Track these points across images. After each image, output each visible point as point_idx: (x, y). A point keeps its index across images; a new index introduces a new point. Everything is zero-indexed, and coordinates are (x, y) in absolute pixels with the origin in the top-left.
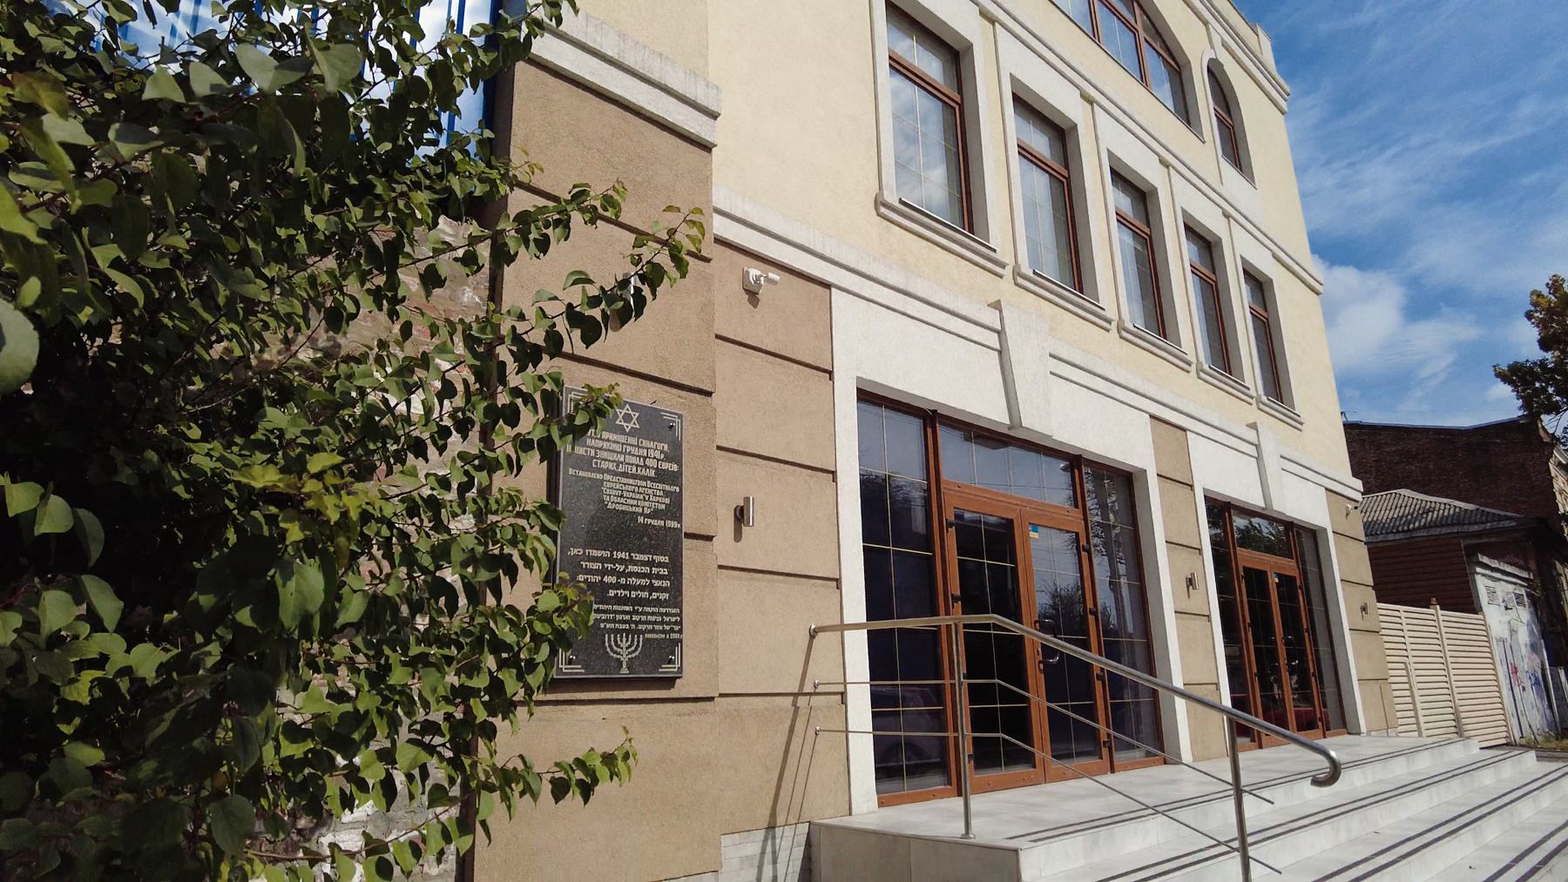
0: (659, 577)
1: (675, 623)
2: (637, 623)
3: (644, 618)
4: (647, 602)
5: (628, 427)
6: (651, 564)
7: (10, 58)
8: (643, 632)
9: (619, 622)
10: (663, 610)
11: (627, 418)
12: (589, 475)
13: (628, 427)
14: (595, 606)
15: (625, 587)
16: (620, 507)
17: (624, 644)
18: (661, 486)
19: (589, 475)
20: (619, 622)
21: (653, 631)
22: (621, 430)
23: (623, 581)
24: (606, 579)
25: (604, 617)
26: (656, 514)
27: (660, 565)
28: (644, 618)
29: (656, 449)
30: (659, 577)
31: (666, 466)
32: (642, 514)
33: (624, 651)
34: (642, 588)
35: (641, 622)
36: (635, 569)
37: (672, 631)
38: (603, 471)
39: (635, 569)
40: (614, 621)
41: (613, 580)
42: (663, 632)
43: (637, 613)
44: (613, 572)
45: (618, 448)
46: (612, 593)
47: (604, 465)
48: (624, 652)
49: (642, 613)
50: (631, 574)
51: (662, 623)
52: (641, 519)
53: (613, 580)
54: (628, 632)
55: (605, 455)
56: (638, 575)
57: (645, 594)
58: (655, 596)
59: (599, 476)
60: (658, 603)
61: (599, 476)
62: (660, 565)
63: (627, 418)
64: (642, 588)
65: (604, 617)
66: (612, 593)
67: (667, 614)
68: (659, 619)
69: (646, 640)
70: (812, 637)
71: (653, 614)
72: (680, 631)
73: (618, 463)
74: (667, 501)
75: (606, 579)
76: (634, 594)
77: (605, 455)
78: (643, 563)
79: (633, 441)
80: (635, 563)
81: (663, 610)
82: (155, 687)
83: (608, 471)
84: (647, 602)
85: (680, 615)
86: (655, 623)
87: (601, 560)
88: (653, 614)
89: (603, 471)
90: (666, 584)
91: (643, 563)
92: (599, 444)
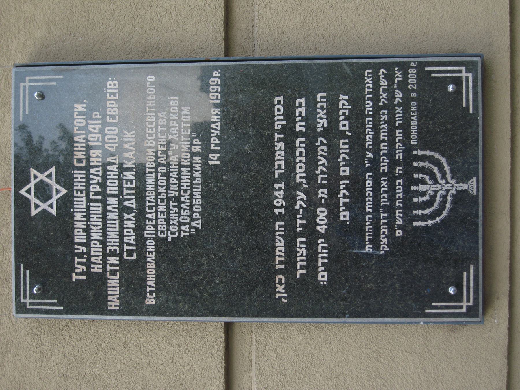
0: (310, 118)
1: (390, 78)
2: (393, 163)
3: (384, 148)
4: (357, 140)
5: (58, 191)
7: (396, 108)
8: (408, 151)
9: (392, 199)
10: (369, 105)
11: (43, 191)
12: (151, 266)
13: (58, 191)
14: (368, 249)
15: (334, 191)
16: (198, 202)
17: (429, 188)
18: (150, 118)
19: (151, 266)
20: (392, 199)
21: (406, 128)
23: (322, 193)
24: (322, 228)
25: (384, 230)
27: (289, 114)
28: (384, 148)
30: (310, 118)
32: (205, 158)
33: (440, 187)
34: (333, 154)
35: (391, 155)
36: (301, 169)
37: (403, 85)
38: (141, 241)
39: (301, 169)
40: (391, 209)
41: (322, 213)
42: (405, 105)
43: (375, 162)
45: (97, 211)
46: (345, 216)
47: (130, 237)
48: (442, 186)
49: (376, 151)
50: (311, 177)
51: (390, 107)
52: (214, 159)
53: (322, 213)
54: (410, 181)
55: (113, 235)
56: (312, 162)
57: (343, 145)
58: (344, 125)
59: (151, 245)
60: (357, 116)
61: (151, 245)
62: (289, 114)
64: (333, 154)
65: (384, 230)
66: (345, 216)
67: (376, 99)
68: (384, 115)
69: (423, 144)
70: (480, 56)
71: (376, 128)
72: (404, 67)
73: (123, 210)
74: (174, 101)
75: (322, 228)
76: (345, 171)
77: (113, 235)
78: (290, 149)
79: (79, 177)
80: (291, 167)
81: (369, 105)
82: (471, 114)
83: (139, 229)
84: (357, 140)
85: (376, 68)
86: (391, 122)
87: (290, 237)
88: (376, 128)
89: (141, 241)
91: (290, 149)
92: (96, 248)
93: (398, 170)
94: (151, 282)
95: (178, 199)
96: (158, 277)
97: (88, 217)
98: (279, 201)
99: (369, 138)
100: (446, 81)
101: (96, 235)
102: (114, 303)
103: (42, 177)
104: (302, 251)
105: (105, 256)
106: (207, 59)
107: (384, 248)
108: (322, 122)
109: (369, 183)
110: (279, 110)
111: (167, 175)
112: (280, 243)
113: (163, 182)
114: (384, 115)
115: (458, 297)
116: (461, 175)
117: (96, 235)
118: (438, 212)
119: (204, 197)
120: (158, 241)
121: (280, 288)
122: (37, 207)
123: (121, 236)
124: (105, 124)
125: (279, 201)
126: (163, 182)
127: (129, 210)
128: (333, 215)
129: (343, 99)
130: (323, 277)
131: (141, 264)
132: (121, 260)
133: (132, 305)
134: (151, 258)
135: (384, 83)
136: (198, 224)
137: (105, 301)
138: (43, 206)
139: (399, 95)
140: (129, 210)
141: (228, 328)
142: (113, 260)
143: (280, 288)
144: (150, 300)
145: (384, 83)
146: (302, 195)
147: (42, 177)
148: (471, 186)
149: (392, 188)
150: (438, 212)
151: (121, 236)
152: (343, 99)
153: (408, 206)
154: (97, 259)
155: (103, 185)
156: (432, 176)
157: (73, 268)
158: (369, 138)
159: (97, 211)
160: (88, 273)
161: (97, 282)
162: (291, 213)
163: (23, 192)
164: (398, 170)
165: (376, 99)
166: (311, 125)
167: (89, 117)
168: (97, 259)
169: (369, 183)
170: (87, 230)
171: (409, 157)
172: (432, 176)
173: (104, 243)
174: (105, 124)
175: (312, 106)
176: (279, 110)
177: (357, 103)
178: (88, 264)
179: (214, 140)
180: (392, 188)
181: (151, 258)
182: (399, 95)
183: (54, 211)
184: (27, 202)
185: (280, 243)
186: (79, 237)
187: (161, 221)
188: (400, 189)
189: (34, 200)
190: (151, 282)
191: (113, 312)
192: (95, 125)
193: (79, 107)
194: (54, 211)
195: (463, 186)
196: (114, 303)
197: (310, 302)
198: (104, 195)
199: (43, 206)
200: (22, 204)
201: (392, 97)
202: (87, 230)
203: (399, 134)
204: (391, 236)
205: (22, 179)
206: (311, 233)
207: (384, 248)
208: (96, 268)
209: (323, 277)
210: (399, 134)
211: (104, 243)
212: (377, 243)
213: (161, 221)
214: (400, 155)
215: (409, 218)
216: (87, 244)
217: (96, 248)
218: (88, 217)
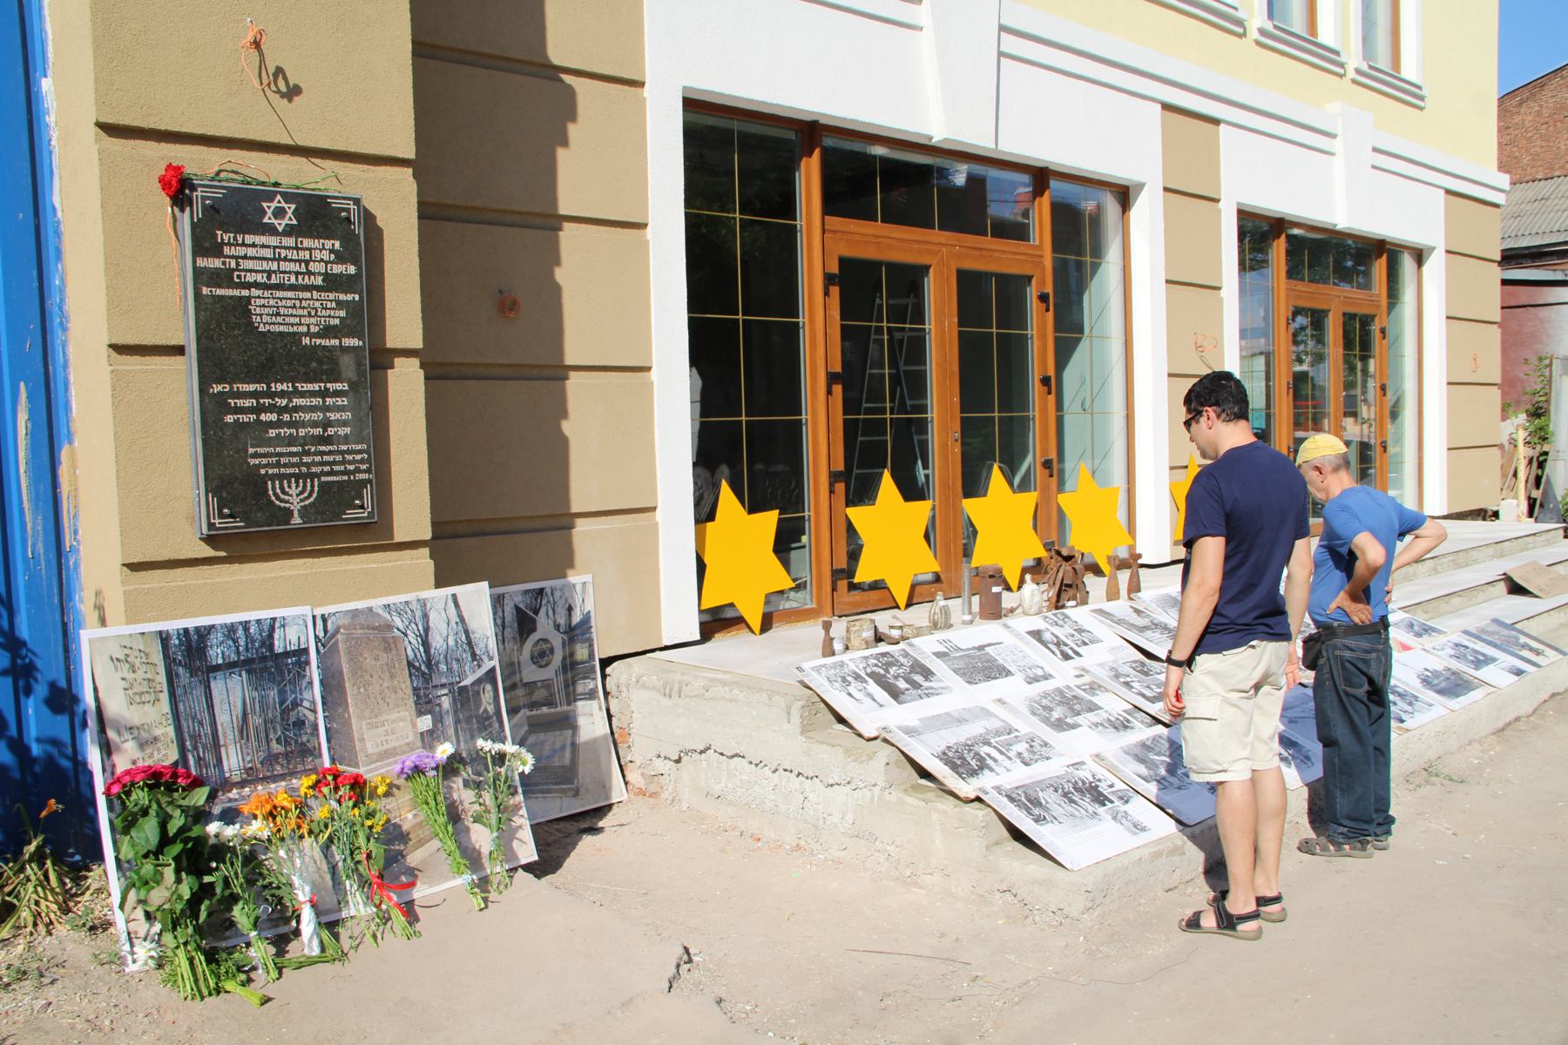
1: (362, 461)
2: (308, 465)
3: (318, 459)
6: (324, 394)
8: (318, 475)
9: (285, 466)
11: (280, 213)
14: (251, 450)
16: (277, 329)
17: (294, 491)
18: (332, 296)
20: (285, 466)
22: (271, 230)
23: (286, 417)
24: (263, 417)
25: (265, 461)
26: (328, 331)
27: (337, 394)
29: (321, 251)
31: (338, 269)
32: (308, 334)
33: (295, 499)
35: (314, 464)
38: (248, 286)
40: (278, 465)
41: (273, 417)
43: (308, 453)
44: (272, 408)
45: (268, 253)
46: (272, 433)
47: (250, 278)
49: (315, 454)
50: (296, 409)
51: (343, 462)
52: (306, 341)
53: (273, 417)
54: (297, 477)
55: (250, 264)
59: (245, 293)
61: (245, 293)
62: (337, 394)
63: (280, 213)
65: (265, 461)
67: (349, 452)
68: (339, 458)
69: (321, 485)
71: (330, 453)
73: (269, 273)
74: (342, 313)
75: (263, 417)
76: (302, 432)
77: (250, 264)
78: (313, 394)
80: (302, 395)
81: (344, 448)
83: (256, 285)
86: (335, 463)
88: (330, 453)
89: (248, 286)
90: (347, 415)
91: (313, 394)
92: (241, 251)
93: (304, 469)
94: (220, 292)
95: (278, 314)
96: (222, 297)
97: (263, 246)
98: (280, 387)
99: (323, 448)
100: (361, 499)
101: (251, 252)
102: (201, 262)
103: (290, 212)
104: (248, 403)
105: (236, 258)
106: (485, 383)
107: (252, 461)
108: (333, 416)
109: (294, 449)
110: (339, 386)
111: (294, 307)
112: (252, 387)
113: (289, 303)
114: (339, 458)
115: (221, 516)
116: (304, 511)
117: (251, 252)
118: (278, 498)
119: (280, 333)
120: (249, 298)
121: (220, 388)
122: (290, 219)
123: (250, 271)
124: (327, 263)
125: (280, 387)
126: (289, 303)
127: (269, 278)
128: (271, 425)
129: (348, 430)
130: (230, 419)
131: (231, 284)
132: (233, 270)
133: (200, 275)
134: (236, 293)
135: (359, 457)
136: (262, 329)
137: (203, 255)
138: (269, 212)
139: (352, 467)
140: (269, 278)
141: (179, 350)
142: (233, 265)
143: (220, 388)
144: (205, 291)
145: (359, 457)
146: (284, 402)
147: (290, 212)
148: (297, 520)
149: (293, 465)
150: (278, 498)
151: (250, 271)
152: (348, 430)
153: (281, 477)
154: (233, 251)
155: (285, 259)
156: (302, 492)
157: (226, 231)
158: (323, 448)
159: (268, 253)
160: (223, 244)
161: (216, 250)
162: (272, 395)
163: (279, 197)
164: (304, 469)
165: (349, 452)
166: (328, 409)
167: (332, 251)
168: (233, 251)
169: (294, 449)
170: (254, 245)
171: (312, 476)
172: (302, 492)
173: (245, 257)
174: (327, 263)
175: (342, 409)
176: (339, 386)
177: (346, 439)
178: (229, 244)
179: (318, 341)
180: (293, 465)
181: (236, 293)
182: (352, 467)
183: (266, 220)
184: (272, 201)
185: (252, 387)
186: (249, 239)
187: (262, 302)
188: (291, 471)
189: (274, 205)
190: (220, 292)
191: (194, 262)
192: (325, 255)
193: (337, 245)
194: (266, 220)
195: (296, 514)
196: (201, 262)
197: (212, 412)
198: (279, 260)
199: (269, 212)
200: (270, 197)
201: (350, 463)
202: (254, 245)
203: (327, 469)
204: (260, 466)
205: (288, 197)
206: (258, 410)
207: (252, 461)
208: (226, 250)
209: (230, 419)
210: (327, 469)
211: (245, 257)
212: (258, 457)
213: (262, 302)
214: (314, 470)
215: (273, 478)
216: (243, 245)
217: (241, 251)
218: (263, 246)
